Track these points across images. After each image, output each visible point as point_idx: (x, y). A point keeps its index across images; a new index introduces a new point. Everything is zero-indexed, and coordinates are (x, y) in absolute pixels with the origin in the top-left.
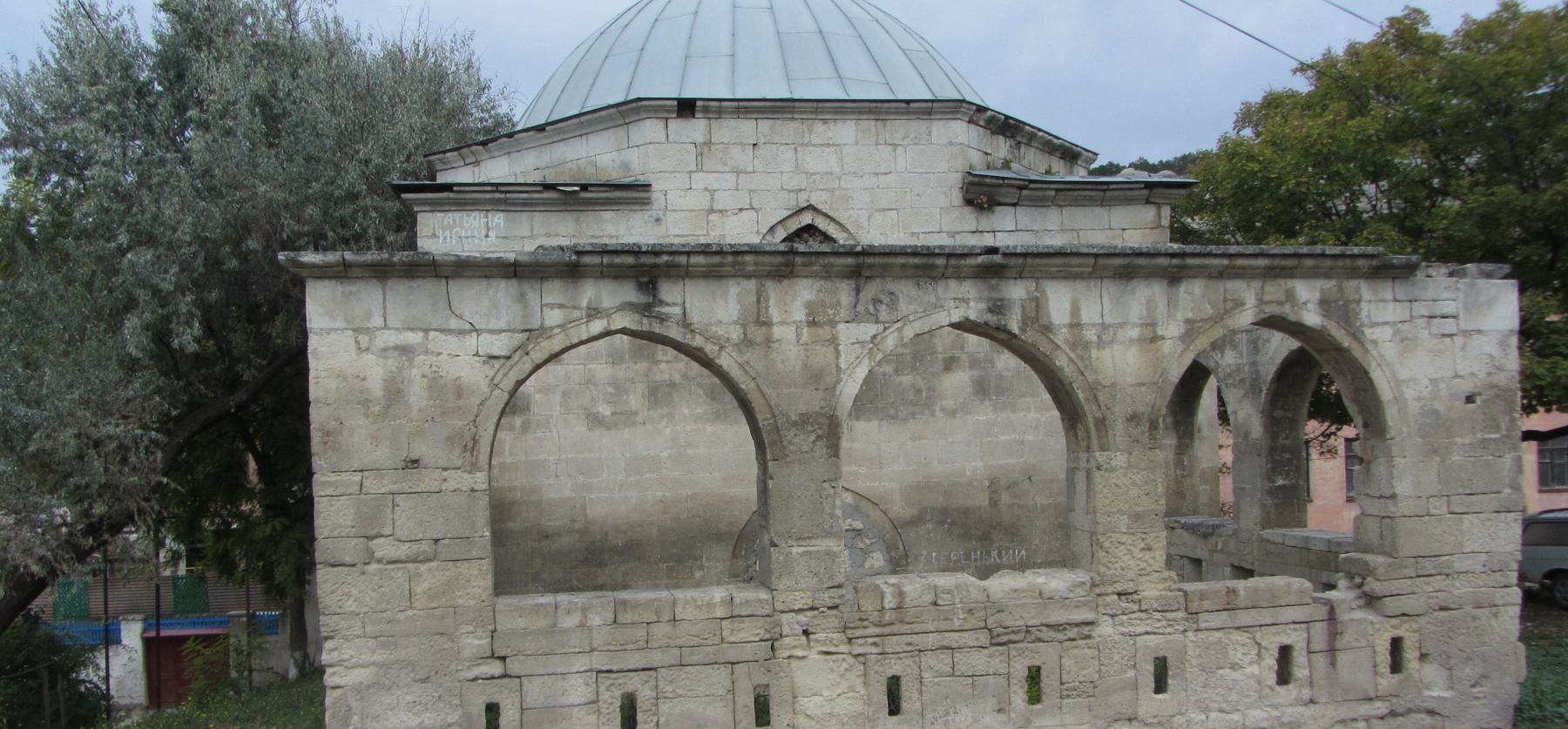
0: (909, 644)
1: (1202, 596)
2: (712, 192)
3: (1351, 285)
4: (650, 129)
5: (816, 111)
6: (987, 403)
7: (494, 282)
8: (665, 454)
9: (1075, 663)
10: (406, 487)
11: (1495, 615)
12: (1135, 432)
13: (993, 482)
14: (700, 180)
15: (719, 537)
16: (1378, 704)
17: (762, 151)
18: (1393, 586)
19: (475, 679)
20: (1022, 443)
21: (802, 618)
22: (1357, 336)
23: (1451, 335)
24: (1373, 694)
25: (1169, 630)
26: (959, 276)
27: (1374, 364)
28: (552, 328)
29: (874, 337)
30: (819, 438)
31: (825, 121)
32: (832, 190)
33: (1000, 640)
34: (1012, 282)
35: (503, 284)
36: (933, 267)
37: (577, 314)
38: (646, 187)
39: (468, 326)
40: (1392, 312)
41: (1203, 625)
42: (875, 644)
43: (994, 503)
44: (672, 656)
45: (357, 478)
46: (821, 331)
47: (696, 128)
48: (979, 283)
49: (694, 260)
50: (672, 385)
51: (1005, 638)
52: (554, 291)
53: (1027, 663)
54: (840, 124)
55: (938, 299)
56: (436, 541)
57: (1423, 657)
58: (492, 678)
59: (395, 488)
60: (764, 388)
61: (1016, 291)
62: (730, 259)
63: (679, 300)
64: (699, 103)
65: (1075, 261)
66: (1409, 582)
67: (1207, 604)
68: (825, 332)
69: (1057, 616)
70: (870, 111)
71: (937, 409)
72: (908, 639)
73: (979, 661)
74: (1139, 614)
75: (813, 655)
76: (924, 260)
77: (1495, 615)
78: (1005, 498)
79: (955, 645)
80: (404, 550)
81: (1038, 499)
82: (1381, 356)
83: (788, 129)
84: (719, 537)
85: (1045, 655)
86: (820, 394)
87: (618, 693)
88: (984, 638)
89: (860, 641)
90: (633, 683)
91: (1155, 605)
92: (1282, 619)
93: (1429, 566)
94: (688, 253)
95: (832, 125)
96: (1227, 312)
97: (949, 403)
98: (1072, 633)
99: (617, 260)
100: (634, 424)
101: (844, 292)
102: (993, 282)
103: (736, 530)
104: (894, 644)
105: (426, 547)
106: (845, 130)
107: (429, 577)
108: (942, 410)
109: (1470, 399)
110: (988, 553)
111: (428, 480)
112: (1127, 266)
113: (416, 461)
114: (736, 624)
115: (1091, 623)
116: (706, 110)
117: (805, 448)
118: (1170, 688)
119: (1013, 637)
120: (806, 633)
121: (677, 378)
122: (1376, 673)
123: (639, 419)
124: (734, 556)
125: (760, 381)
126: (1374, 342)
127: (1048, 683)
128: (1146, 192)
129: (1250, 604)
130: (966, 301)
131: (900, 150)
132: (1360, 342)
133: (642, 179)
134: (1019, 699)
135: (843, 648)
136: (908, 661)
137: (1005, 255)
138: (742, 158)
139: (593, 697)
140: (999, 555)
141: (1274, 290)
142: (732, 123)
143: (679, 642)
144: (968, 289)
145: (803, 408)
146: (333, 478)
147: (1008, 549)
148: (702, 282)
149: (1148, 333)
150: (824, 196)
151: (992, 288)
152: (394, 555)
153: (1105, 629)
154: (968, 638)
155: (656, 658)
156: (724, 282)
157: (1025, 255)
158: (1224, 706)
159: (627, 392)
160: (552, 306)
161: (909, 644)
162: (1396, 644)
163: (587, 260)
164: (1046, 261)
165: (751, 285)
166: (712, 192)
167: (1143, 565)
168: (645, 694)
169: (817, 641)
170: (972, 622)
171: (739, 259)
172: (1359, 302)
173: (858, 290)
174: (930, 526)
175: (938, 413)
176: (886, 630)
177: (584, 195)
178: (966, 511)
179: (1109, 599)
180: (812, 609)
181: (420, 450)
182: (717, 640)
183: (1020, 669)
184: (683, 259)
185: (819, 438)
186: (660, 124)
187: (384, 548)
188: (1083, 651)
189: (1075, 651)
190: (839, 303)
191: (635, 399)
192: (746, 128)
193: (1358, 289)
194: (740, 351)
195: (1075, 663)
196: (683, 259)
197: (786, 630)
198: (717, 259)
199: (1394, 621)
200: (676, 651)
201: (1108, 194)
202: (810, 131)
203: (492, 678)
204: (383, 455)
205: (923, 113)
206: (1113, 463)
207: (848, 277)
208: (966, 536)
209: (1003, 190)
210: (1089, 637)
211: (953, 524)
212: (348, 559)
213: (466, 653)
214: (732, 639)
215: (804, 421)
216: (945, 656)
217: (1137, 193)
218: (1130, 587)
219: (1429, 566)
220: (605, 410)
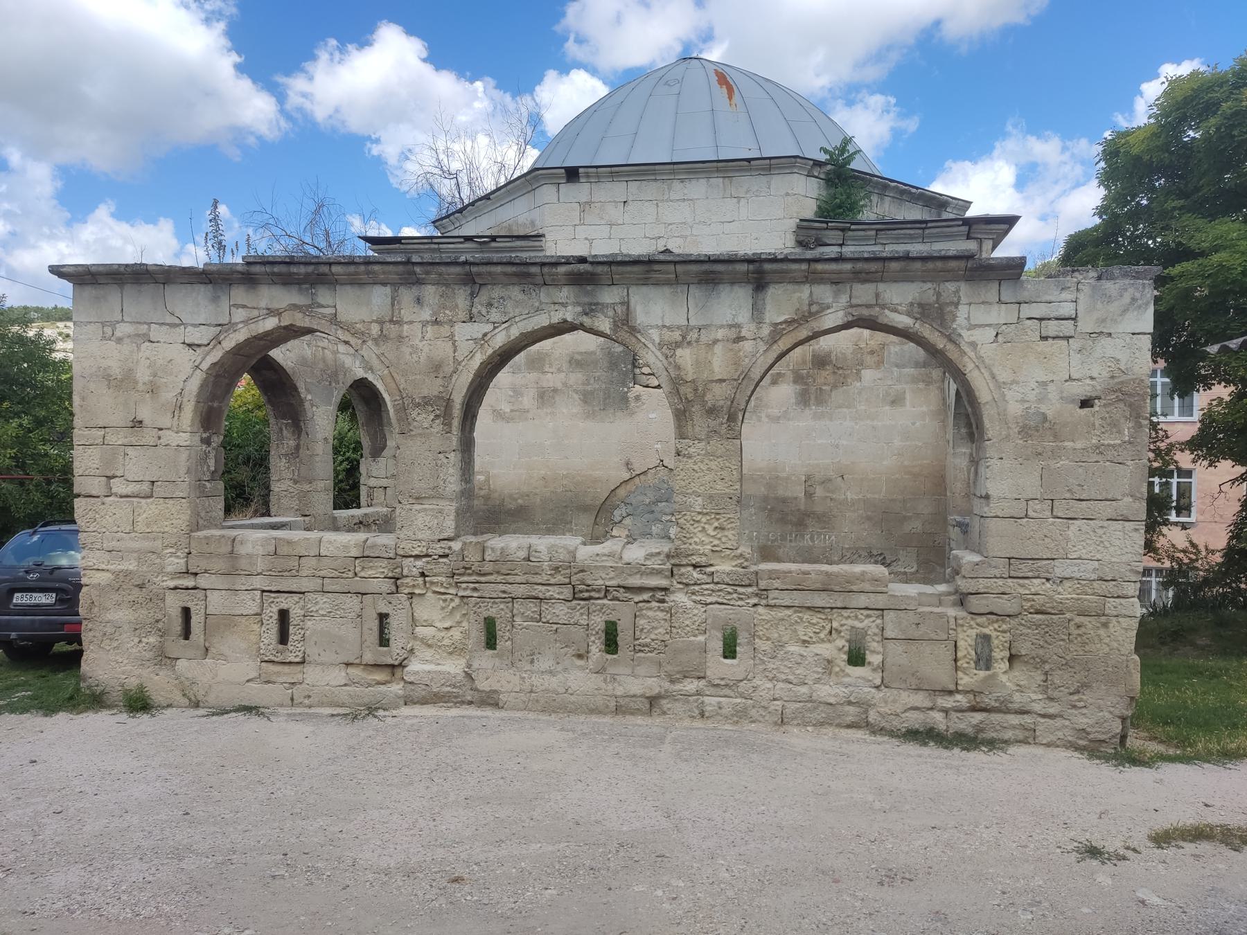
0: (504, 592)
1: (772, 575)
2: (591, 241)
3: (951, 286)
4: (547, 193)
5: (673, 172)
6: (807, 411)
7: (197, 287)
8: (548, 443)
9: (652, 622)
10: (134, 440)
11: (1105, 625)
12: (713, 423)
13: (808, 478)
14: (582, 232)
15: (585, 509)
16: (959, 697)
17: (629, 207)
18: (981, 585)
19: (176, 588)
20: (837, 446)
21: (419, 563)
22: (952, 339)
23: (1067, 338)
24: (952, 687)
25: (740, 603)
26: (555, 284)
27: (970, 366)
28: (237, 324)
29: (485, 335)
30: (437, 416)
31: (682, 181)
32: (686, 237)
33: (580, 594)
34: (606, 288)
35: (202, 288)
36: (528, 275)
37: (256, 313)
38: (543, 236)
39: (178, 321)
40: (998, 315)
41: (772, 602)
42: (475, 589)
43: (809, 495)
44: (314, 584)
45: (102, 432)
46: (442, 329)
47: (580, 191)
48: (576, 288)
49: (335, 269)
50: (555, 390)
51: (586, 595)
52: (239, 294)
53: (605, 618)
54: (694, 182)
55: (541, 303)
56: (153, 482)
57: (1012, 658)
58: (187, 589)
59: (126, 441)
60: (395, 375)
61: (610, 296)
62: (362, 268)
63: (330, 302)
64: (581, 170)
66: (1000, 582)
67: (777, 584)
68: (445, 330)
69: (636, 581)
70: (718, 170)
71: (763, 415)
72: (503, 587)
73: (560, 611)
74: (711, 586)
75: (429, 594)
76: (522, 269)
77: (1105, 625)
78: (819, 492)
79: (541, 596)
80: (131, 489)
81: (848, 494)
82: (980, 358)
83: (650, 189)
84: (585, 509)
85: (622, 613)
86: (439, 381)
87: (275, 609)
88: (567, 592)
89: (464, 585)
90: (285, 602)
91: (727, 580)
92: (854, 604)
93: (1025, 569)
94: (330, 264)
95: (687, 184)
96: (811, 314)
97: (775, 412)
98: (646, 596)
99: (276, 269)
100: (526, 419)
101: (461, 297)
102: (589, 288)
103: (598, 503)
104: (487, 590)
106: (697, 188)
107: (149, 509)
108: (768, 416)
109: (1086, 403)
110: (803, 536)
111: (149, 437)
112: (706, 272)
113: (141, 422)
114: (367, 563)
115: (665, 589)
116: (588, 176)
117: (426, 425)
118: (738, 655)
119: (593, 594)
120: (423, 575)
121: (559, 385)
122: (957, 669)
123: (530, 415)
124: (595, 523)
125: (392, 369)
126: (973, 345)
127: (623, 638)
128: (965, 228)
129: (819, 586)
130: (564, 305)
131: (743, 202)
132: (957, 345)
133: (541, 232)
134: (596, 648)
135: (452, 591)
136: (502, 606)
137: (592, 263)
138: (615, 213)
139: (256, 610)
140: (812, 538)
141: (863, 293)
142: (609, 185)
143: (322, 573)
144: (565, 293)
145: (425, 392)
146: (87, 432)
147: (819, 534)
148: (348, 288)
149: (732, 334)
150: (679, 241)
151: (587, 293)
152: (124, 491)
153: (680, 598)
154: (553, 592)
155: (305, 584)
156: (368, 288)
157: (610, 263)
158: (791, 677)
159: (522, 395)
160: (237, 306)
161: (504, 592)
162: (186, 612)
163: (257, 269)
164: (629, 268)
165: (388, 290)
166: (591, 241)
167: (716, 542)
168: (295, 613)
169: (432, 583)
170: (559, 578)
171: (370, 267)
172: (957, 305)
173: (473, 295)
174: (753, 511)
175: (765, 419)
176: (483, 579)
177: (493, 244)
178: (784, 501)
179: (683, 570)
180: (427, 556)
181: (145, 413)
182: (351, 574)
183: (598, 621)
184: (325, 269)
185: (437, 416)
186: (553, 188)
187: (118, 486)
188: (654, 613)
189: (650, 613)
190: (457, 306)
191: (528, 401)
192: (618, 190)
193: (957, 291)
194: (377, 344)
195: (652, 622)
196: (325, 269)
197: (405, 572)
198: (352, 269)
199: (980, 620)
200: (319, 581)
201: (927, 231)
202: (669, 189)
203: (187, 589)
204: (118, 418)
205: (763, 169)
206: (692, 450)
207: (465, 284)
208: (783, 520)
209: (827, 232)
210: (663, 601)
211: (772, 510)
212: (94, 493)
213: (169, 569)
214: (362, 574)
215: (426, 402)
216: (532, 607)
217: (956, 229)
218: (703, 560)
219: (1025, 569)
220: (506, 408)
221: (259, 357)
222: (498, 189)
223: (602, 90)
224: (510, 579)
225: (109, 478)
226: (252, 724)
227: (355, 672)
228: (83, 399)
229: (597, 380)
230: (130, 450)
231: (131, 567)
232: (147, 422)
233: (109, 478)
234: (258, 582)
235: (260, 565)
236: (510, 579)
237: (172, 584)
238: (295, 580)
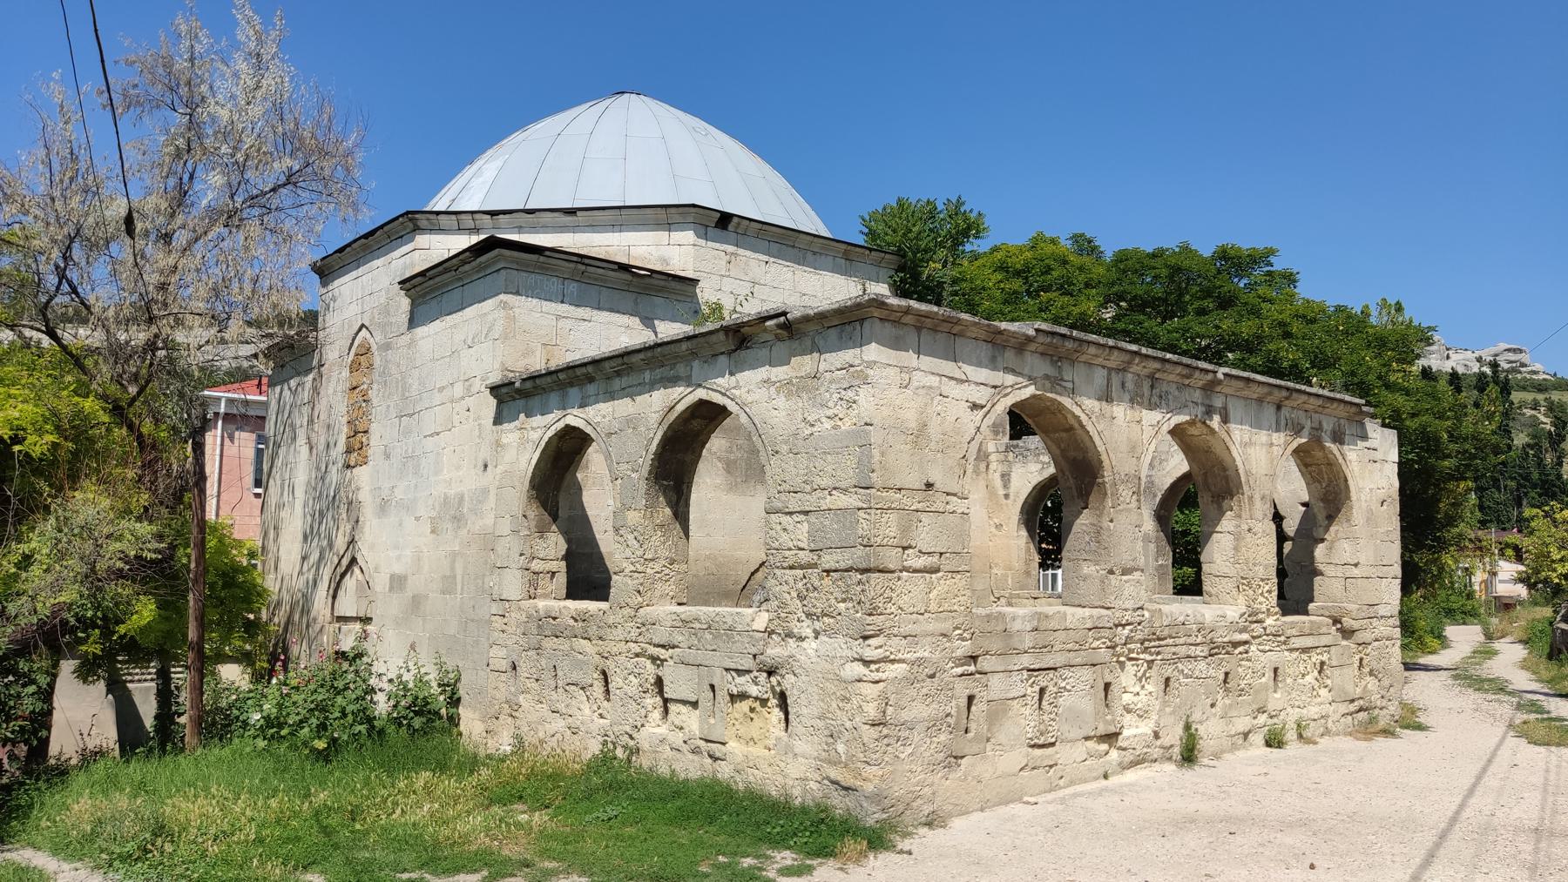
65: (607, 365)
67: (1294, 632)
72: (1174, 649)
105: (935, 559)
221: (588, 430)
222: (550, 373)
223: (656, 322)
224: (1178, 641)
225: (904, 548)
226: (249, 479)
227: (1091, 744)
228: (883, 454)
229: (740, 448)
230: (923, 516)
231: (926, 654)
232: (937, 485)
233: (904, 548)
234: (1026, 661)
235: (1028, 642)
236: (1178, 641)
237: (959, 670)
238: (1050, 656)
